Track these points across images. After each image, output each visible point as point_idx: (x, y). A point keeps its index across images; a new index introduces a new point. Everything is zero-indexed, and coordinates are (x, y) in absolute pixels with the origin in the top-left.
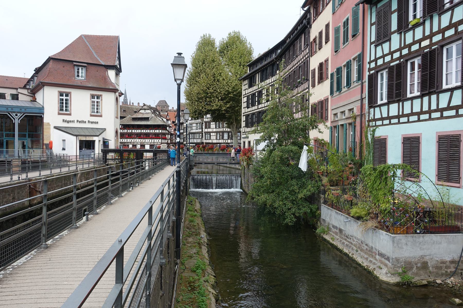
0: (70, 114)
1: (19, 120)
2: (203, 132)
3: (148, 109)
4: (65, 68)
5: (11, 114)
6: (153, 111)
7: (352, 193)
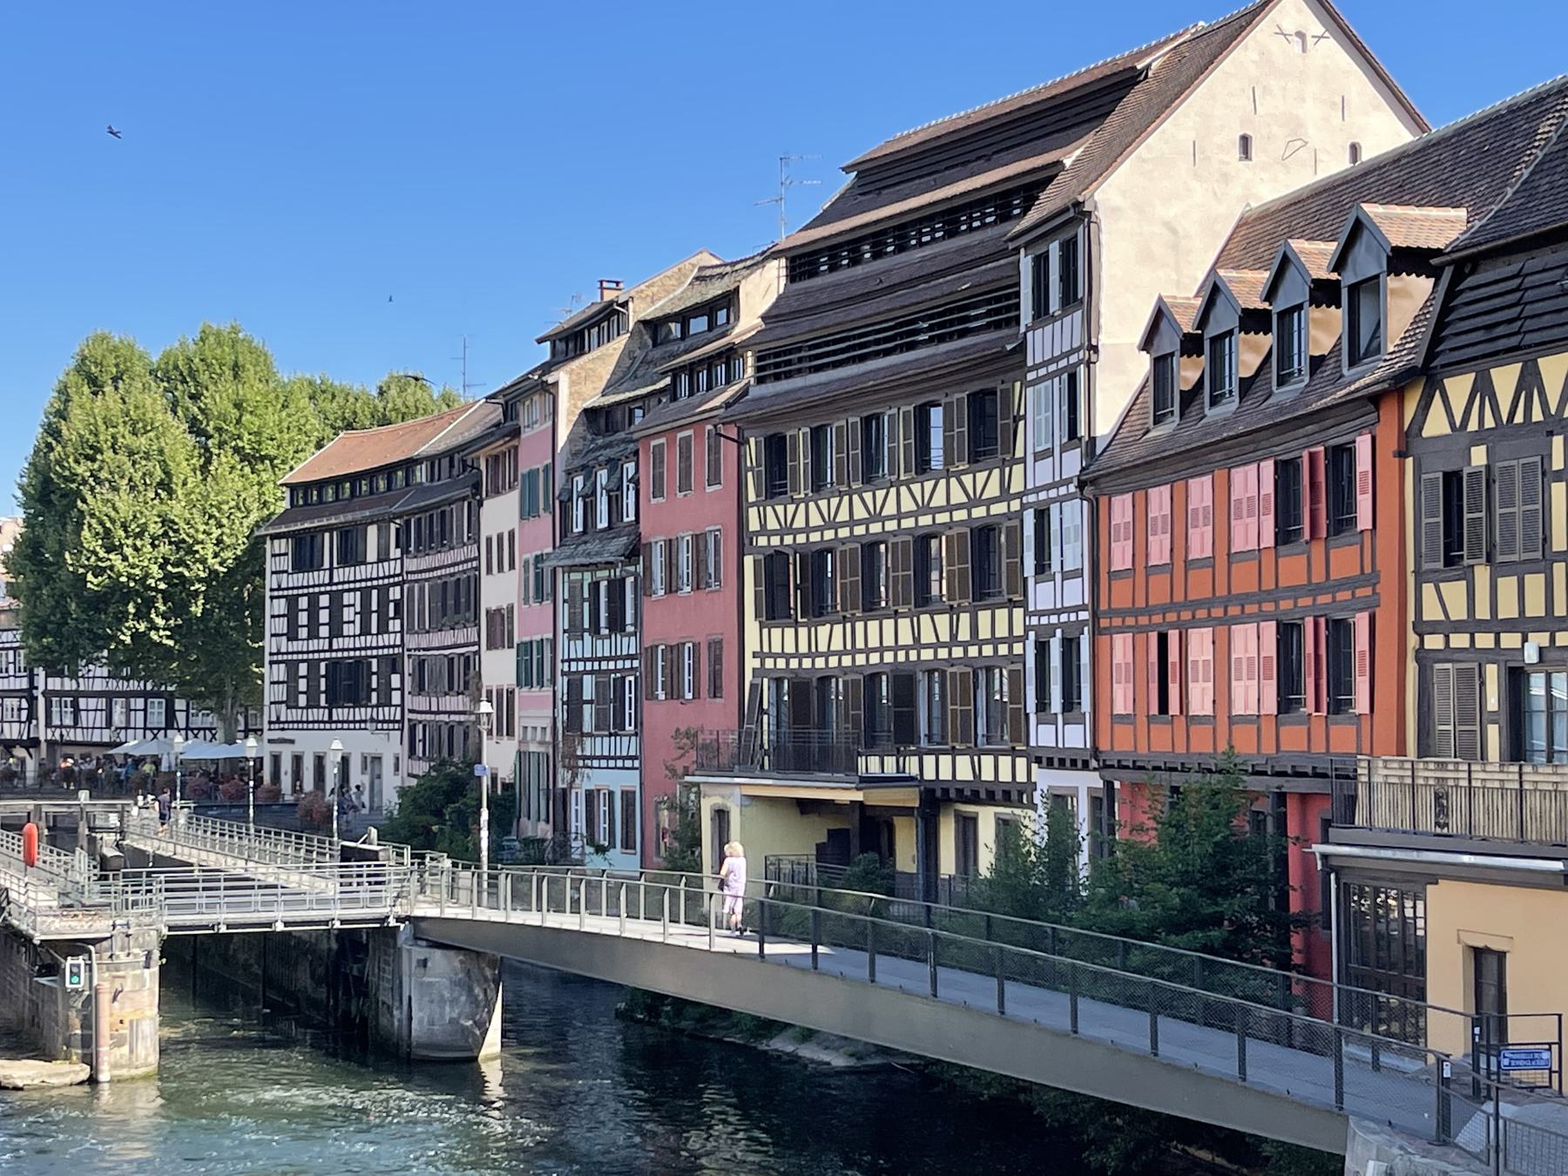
2: (38, 693)
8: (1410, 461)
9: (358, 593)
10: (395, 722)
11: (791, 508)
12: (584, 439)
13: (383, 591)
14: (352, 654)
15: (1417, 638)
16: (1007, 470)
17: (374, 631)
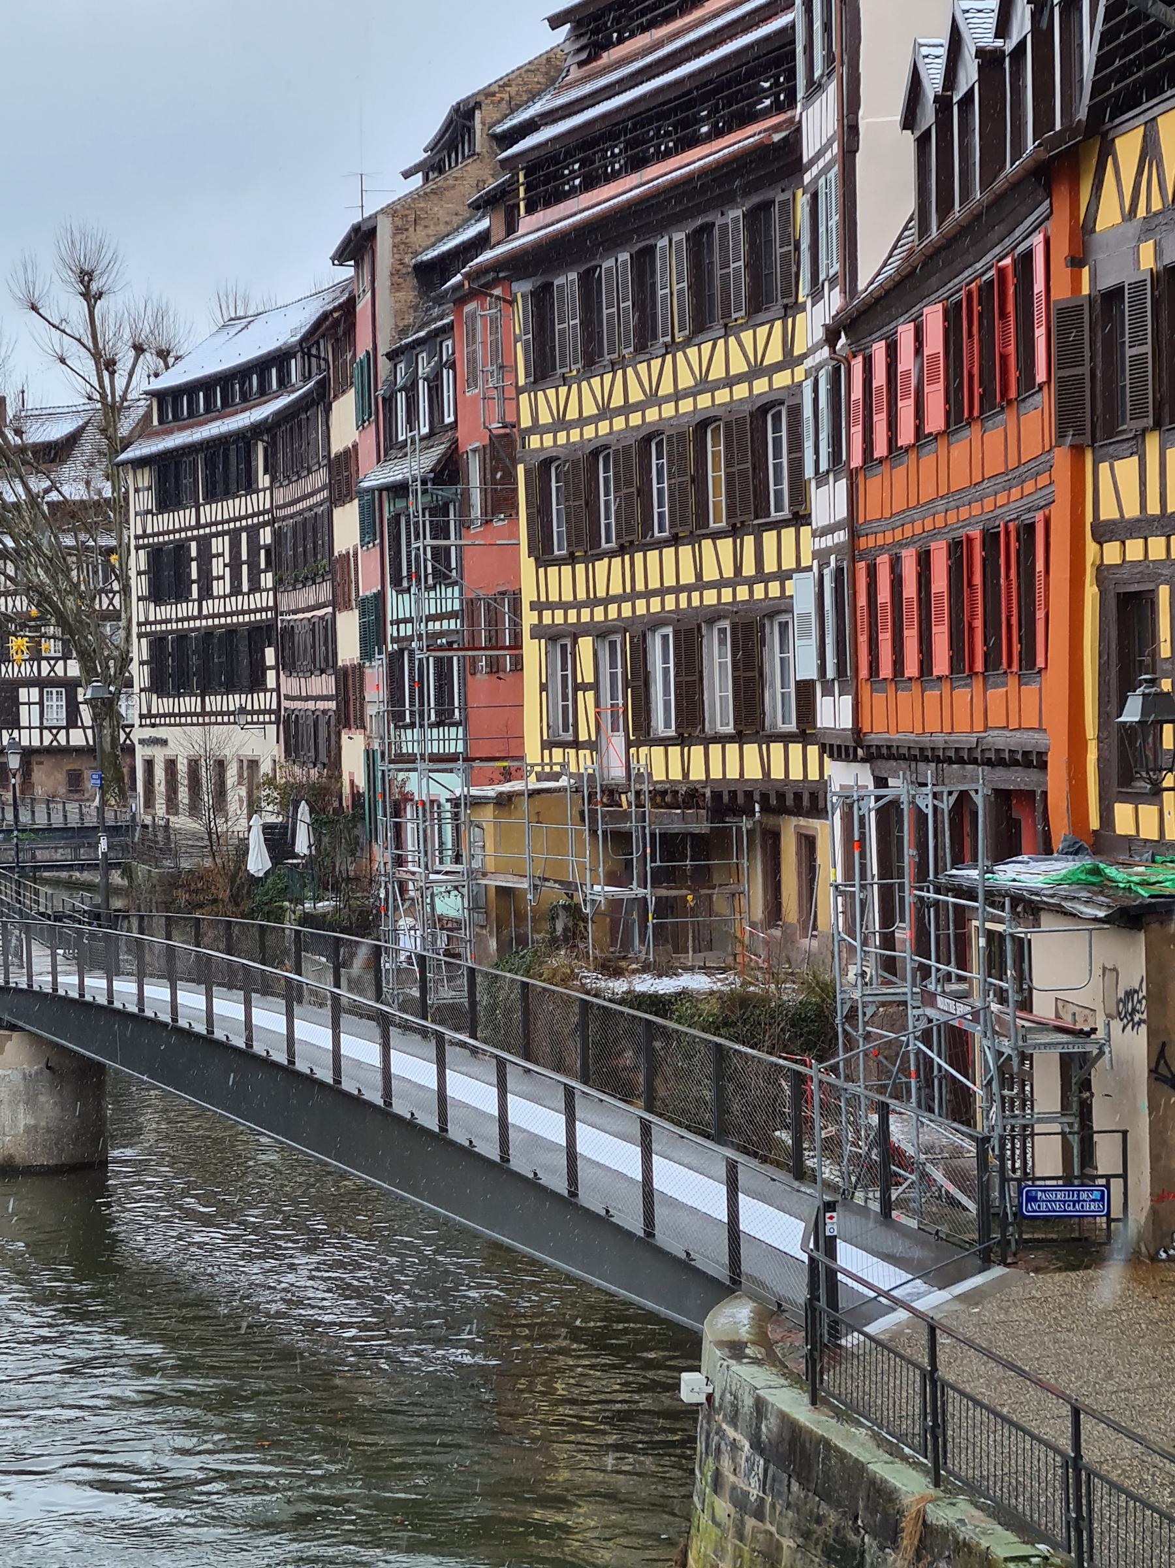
7: (535, 930)
8: (1086, 271)
9: (227, 538)
10: (270, 712)
11: (563, 390)
12: (416, 308)
13: (253, 532)
14: (198, 624)
15: (1097, 547)
16: (790, 320)
17: (245, 588)
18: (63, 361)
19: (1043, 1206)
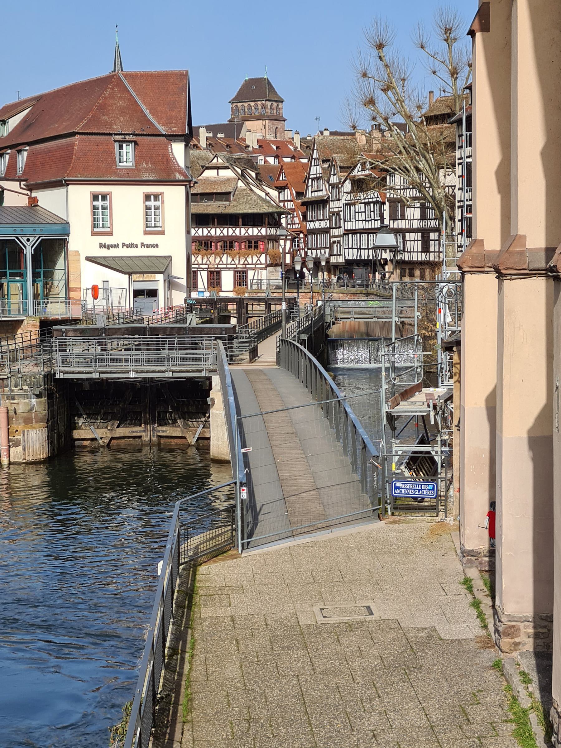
0: (111, 234)
1: (33, 249)
3: (227, 168)
4: (99, 147)
5: (20, 238)
6: (239, 171)
18: (434, 72)
19: (403, 491)
